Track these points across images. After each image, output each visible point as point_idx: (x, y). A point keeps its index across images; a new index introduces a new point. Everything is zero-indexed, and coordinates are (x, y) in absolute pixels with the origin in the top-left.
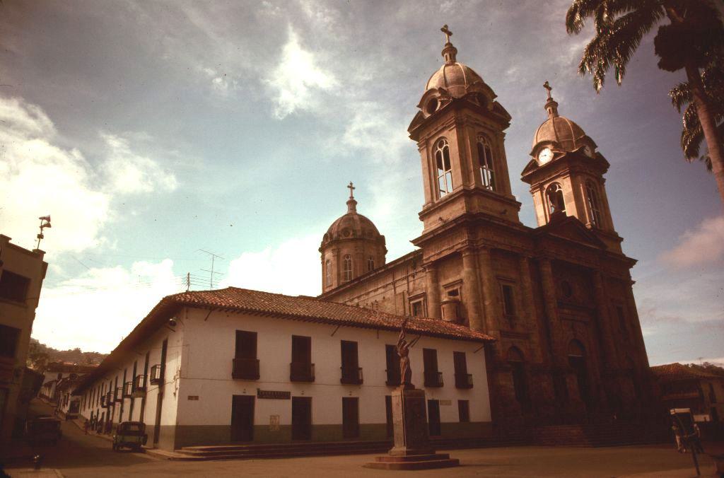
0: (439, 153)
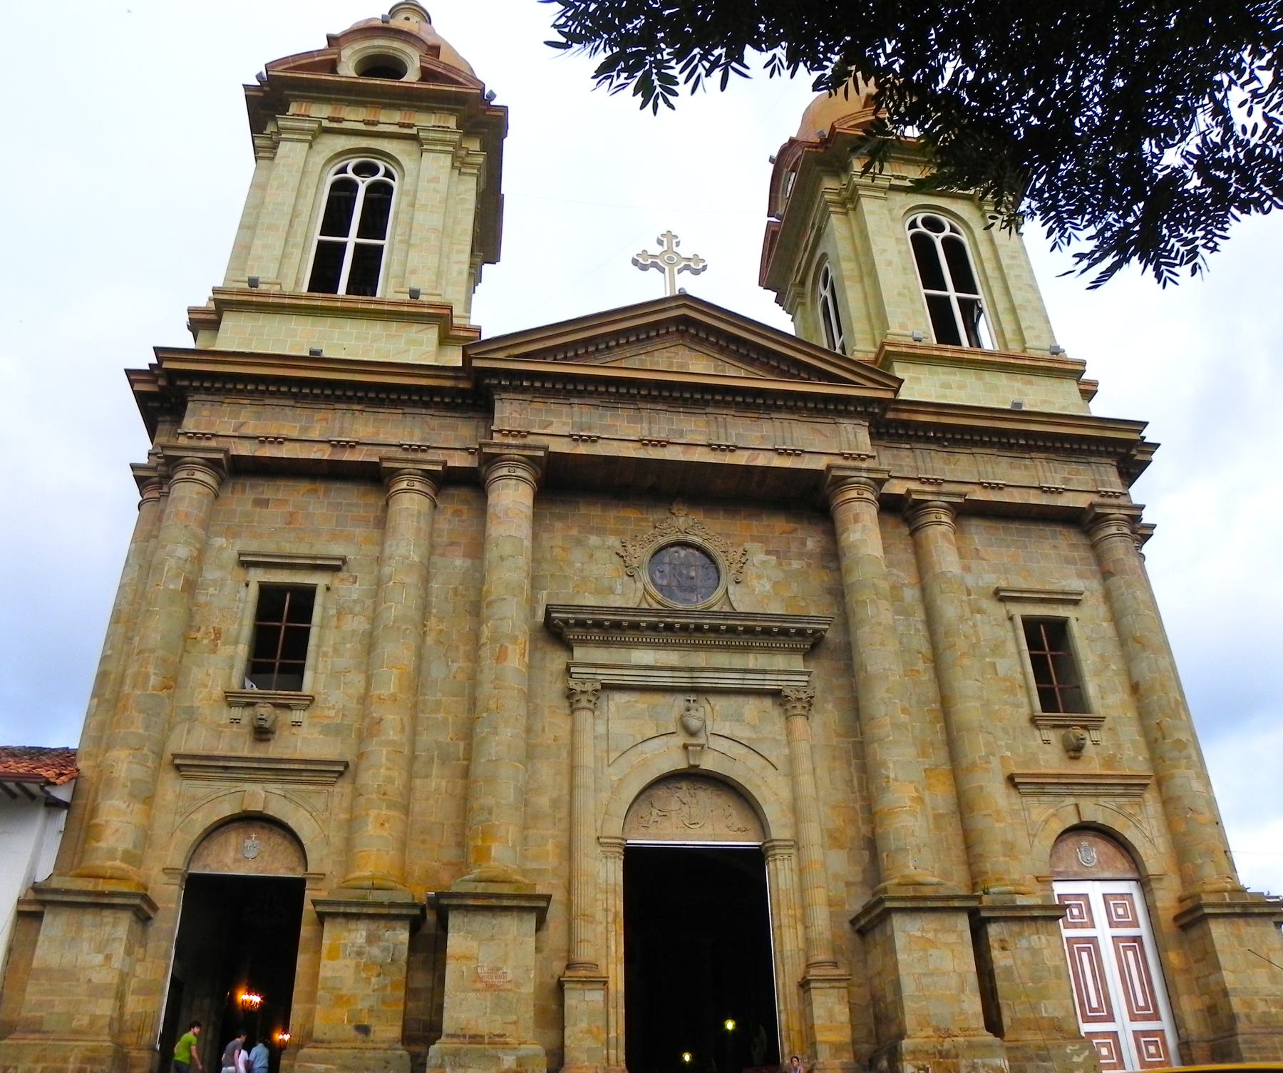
0: (938, 227)
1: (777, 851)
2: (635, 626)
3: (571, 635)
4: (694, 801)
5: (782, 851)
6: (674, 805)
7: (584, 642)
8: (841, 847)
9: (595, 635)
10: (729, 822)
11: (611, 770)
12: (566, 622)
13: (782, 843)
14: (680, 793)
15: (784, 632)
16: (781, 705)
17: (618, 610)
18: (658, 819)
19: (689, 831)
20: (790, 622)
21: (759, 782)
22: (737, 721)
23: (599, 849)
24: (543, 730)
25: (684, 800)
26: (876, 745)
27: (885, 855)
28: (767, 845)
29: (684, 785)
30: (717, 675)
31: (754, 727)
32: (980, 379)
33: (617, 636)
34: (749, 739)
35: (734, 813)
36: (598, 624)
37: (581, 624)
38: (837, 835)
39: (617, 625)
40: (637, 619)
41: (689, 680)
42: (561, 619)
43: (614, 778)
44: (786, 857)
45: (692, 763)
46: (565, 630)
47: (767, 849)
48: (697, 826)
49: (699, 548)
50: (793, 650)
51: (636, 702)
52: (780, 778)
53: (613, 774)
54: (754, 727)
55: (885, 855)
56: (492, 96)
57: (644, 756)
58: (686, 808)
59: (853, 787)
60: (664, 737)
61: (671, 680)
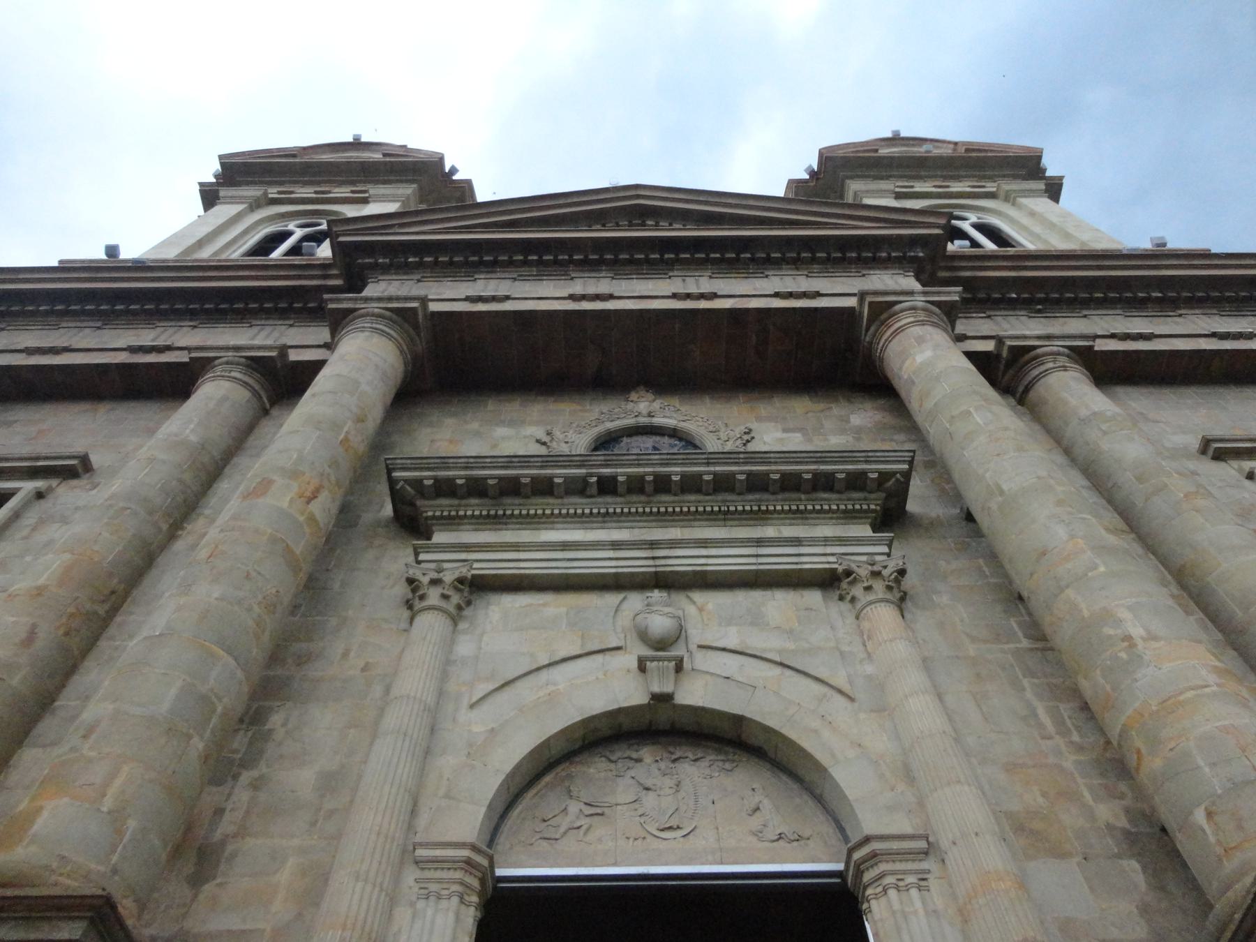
1: (883, 867)
2: (544, 488)
3: (431, 508)
4: (668, 782)
5: (899, 866)
6: (623, 791)
7: (452, 522)
8: (1060, 854)
9: (475, 507)
10: (755, 822)
11: (474, 714)
12: (417, 484)
13: (895, 845)
14: (638, 771)
15: (824, 483)
16: (841, 598)
17: (511, 460)
18: (584, 822)
19: (656, 844)
20: (835, 463)
21: (815, 723)
22: (752, 624)
23: (416, 884)
24: (345, 655)
25: (649, 783)
26: (1070, 593)
27: (1199, 816)
28: (857, 855)
29: (647, 753)
30: (704, 552)
31: (791, 632)
32: (1083, 243)
33: (513, 506)
34: (780, 652)
35: (767, 804)
36: (477, 488)
37: (445, 488)
38: (1037, 825)
39: (511, 488)
40: (549, 471)
41: (651, 562)
42: (406, 481)
43: (477, 729)
44: (911, 879)
45: (656, 689)
46: (419, 503)
47: (859, 873)
48: (680, 833)
49: (674, 433)
50: (849, 516)
51: (544, 605)
52: (862, 716)
53: (477, 723)
54: (791, 632)
55: (1199, 816)
56: (454, 170)
57: (551, 688)
58: (649, 800)
59: (1041, 726)
60: (599, 657)
61: (614, 563)
